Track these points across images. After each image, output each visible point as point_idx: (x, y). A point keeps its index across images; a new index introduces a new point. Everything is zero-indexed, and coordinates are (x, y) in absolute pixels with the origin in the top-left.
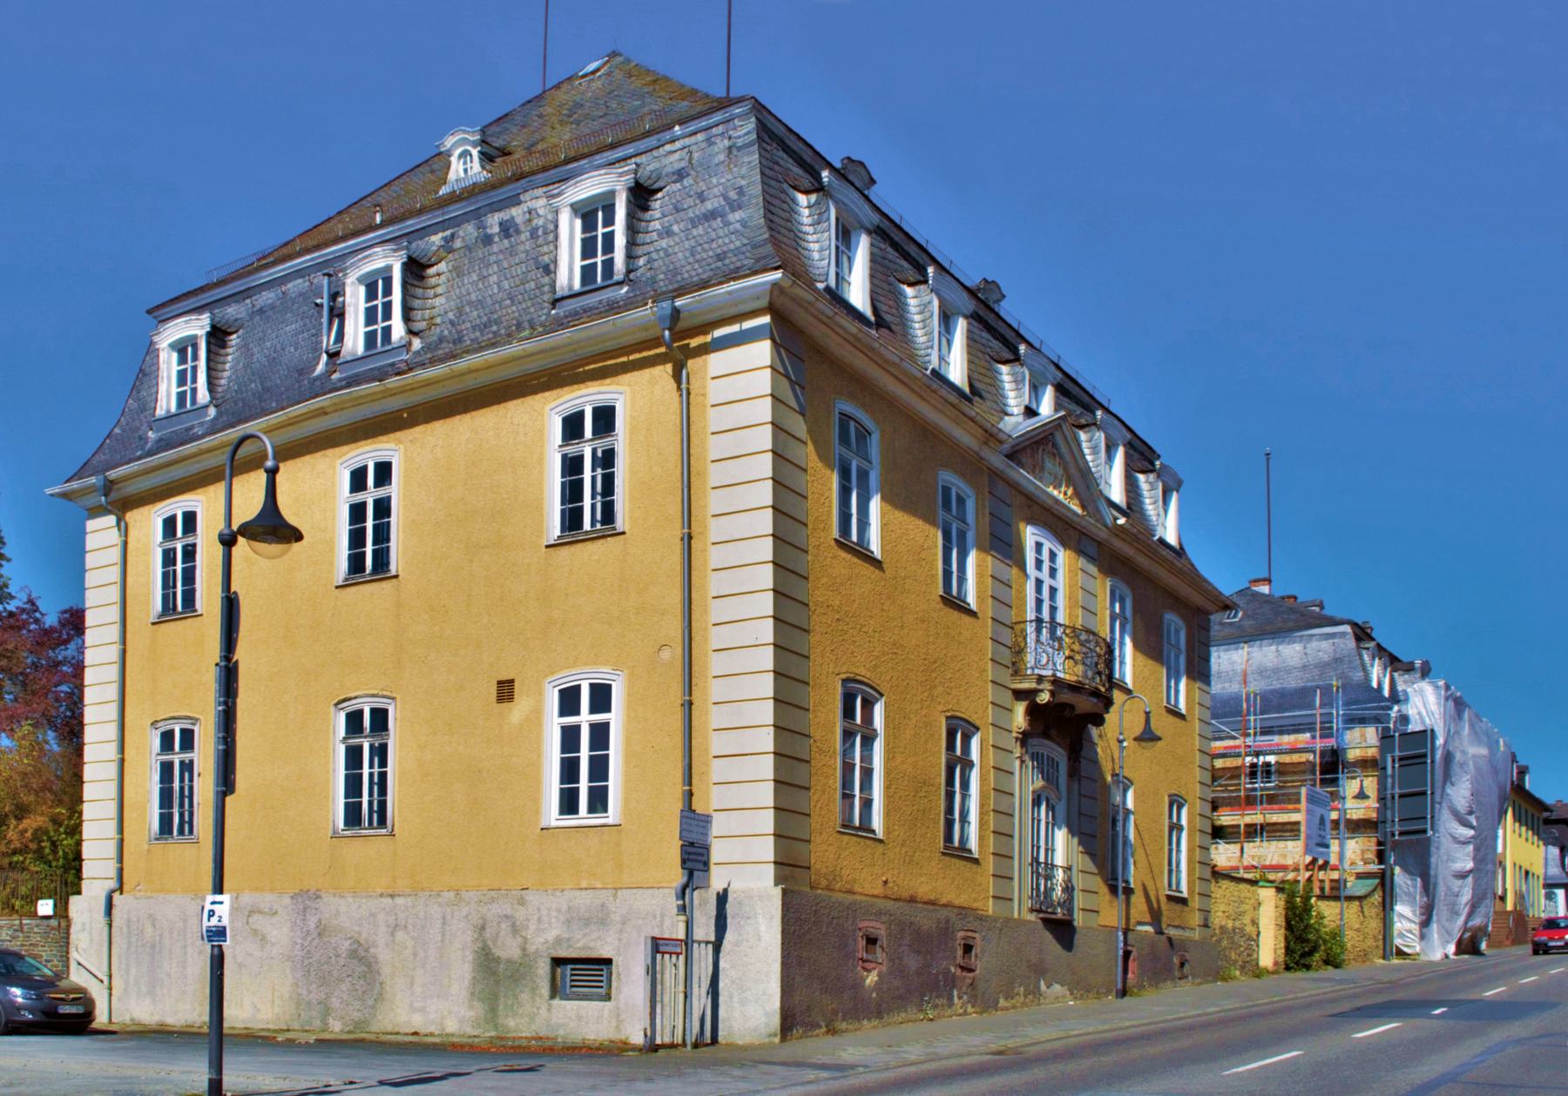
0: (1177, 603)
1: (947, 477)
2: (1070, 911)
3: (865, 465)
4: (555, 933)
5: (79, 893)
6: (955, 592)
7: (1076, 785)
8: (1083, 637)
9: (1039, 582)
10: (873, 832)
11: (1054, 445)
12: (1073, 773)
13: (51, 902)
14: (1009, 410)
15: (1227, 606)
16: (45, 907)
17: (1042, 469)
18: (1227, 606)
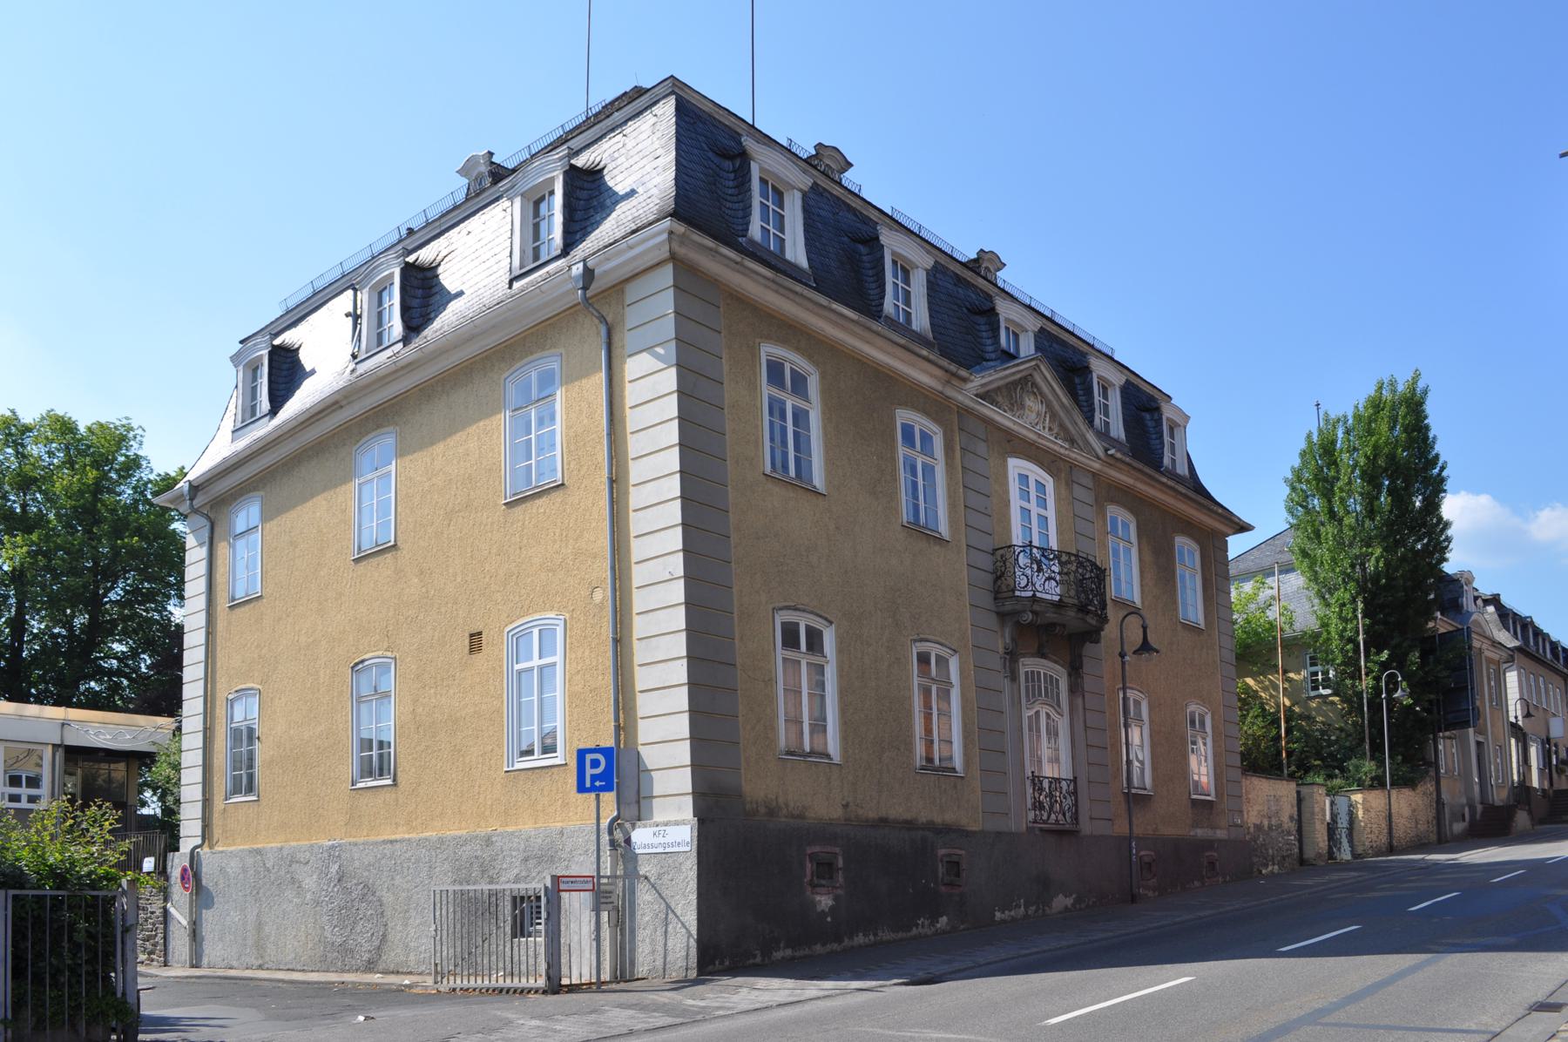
0: (1190, 528)
1: (903, 416)
2: (1076, 817)
3: (802, 404)
4: (516, 871)
5: (177, 849)
6: (922, 520)
7: (1080, 701)
8: (1064, 558)
9: (1026, 512)
10: (828, 756)
11: (1034, 384)
12: (1075, 689)
13: (152, 859)
14: (987, 356)
15: (30, 430)
16: (149, 864)
17: (1022, 406)
18: (30, 430)
